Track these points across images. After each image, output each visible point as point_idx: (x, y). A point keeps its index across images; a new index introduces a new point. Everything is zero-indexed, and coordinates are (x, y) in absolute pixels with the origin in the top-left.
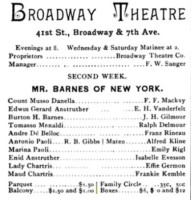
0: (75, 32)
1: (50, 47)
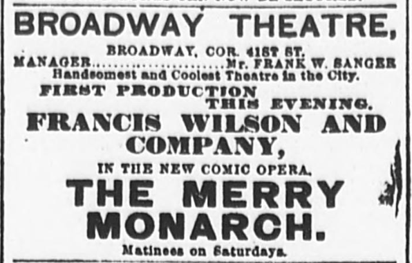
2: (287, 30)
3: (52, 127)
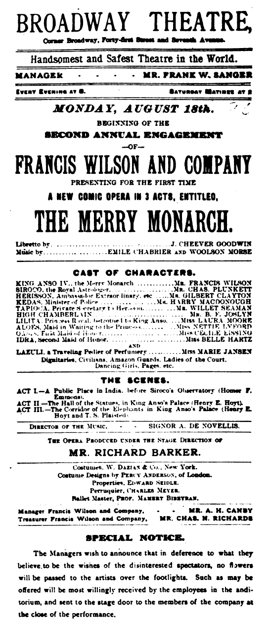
1: (156, 552)
3: (165, 539)
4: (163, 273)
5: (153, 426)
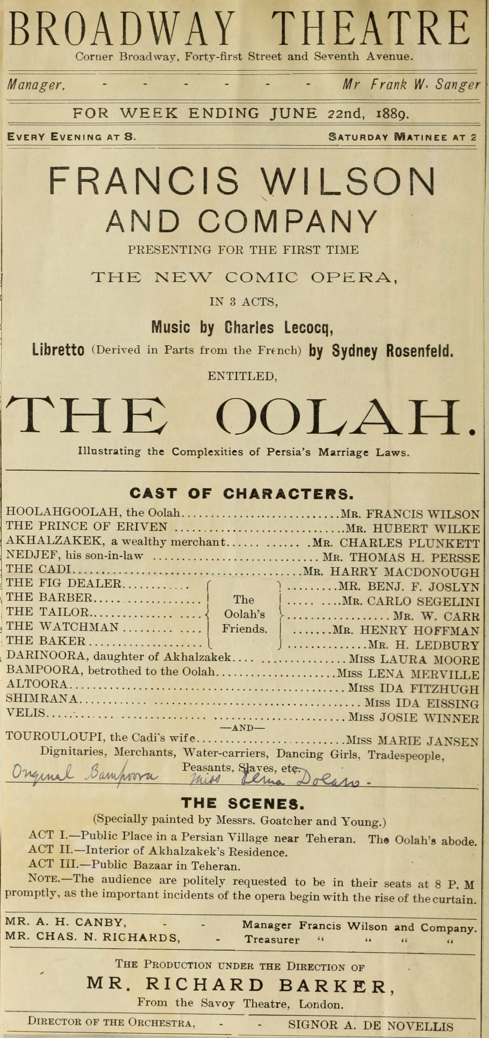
0: (283, 985)
2: (54, 138)
4: (294, 494)
5: (296, 1024)
